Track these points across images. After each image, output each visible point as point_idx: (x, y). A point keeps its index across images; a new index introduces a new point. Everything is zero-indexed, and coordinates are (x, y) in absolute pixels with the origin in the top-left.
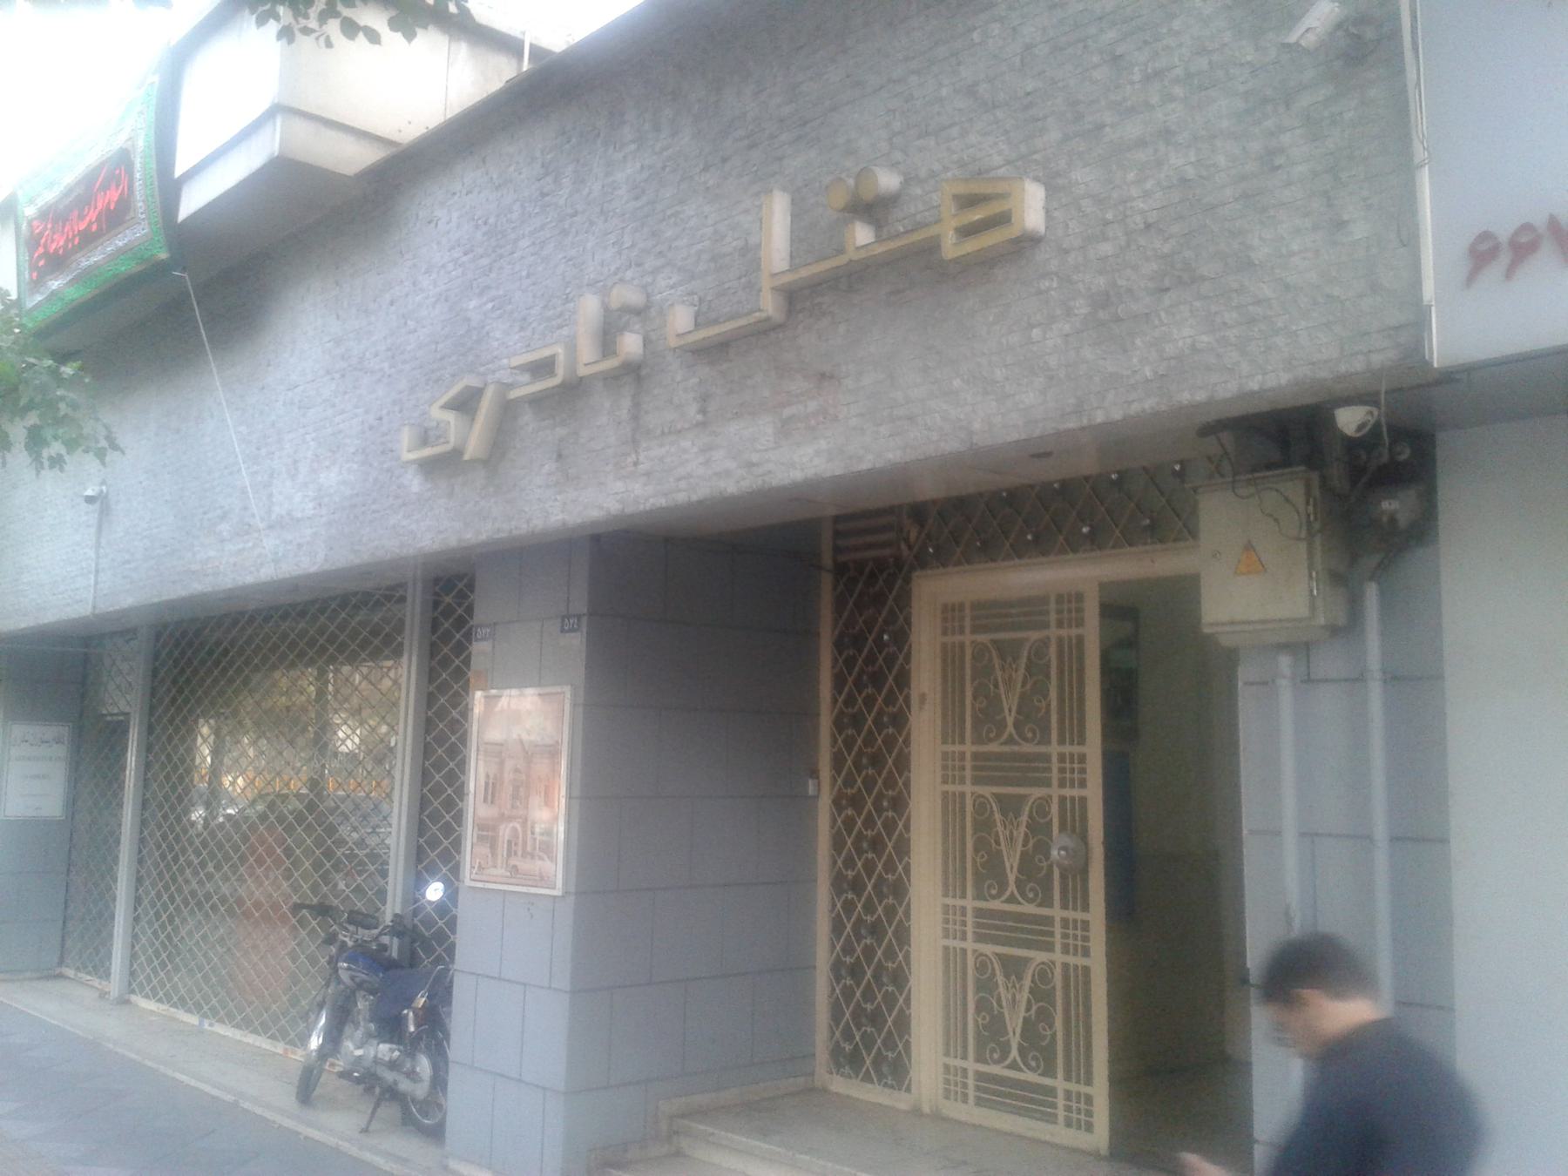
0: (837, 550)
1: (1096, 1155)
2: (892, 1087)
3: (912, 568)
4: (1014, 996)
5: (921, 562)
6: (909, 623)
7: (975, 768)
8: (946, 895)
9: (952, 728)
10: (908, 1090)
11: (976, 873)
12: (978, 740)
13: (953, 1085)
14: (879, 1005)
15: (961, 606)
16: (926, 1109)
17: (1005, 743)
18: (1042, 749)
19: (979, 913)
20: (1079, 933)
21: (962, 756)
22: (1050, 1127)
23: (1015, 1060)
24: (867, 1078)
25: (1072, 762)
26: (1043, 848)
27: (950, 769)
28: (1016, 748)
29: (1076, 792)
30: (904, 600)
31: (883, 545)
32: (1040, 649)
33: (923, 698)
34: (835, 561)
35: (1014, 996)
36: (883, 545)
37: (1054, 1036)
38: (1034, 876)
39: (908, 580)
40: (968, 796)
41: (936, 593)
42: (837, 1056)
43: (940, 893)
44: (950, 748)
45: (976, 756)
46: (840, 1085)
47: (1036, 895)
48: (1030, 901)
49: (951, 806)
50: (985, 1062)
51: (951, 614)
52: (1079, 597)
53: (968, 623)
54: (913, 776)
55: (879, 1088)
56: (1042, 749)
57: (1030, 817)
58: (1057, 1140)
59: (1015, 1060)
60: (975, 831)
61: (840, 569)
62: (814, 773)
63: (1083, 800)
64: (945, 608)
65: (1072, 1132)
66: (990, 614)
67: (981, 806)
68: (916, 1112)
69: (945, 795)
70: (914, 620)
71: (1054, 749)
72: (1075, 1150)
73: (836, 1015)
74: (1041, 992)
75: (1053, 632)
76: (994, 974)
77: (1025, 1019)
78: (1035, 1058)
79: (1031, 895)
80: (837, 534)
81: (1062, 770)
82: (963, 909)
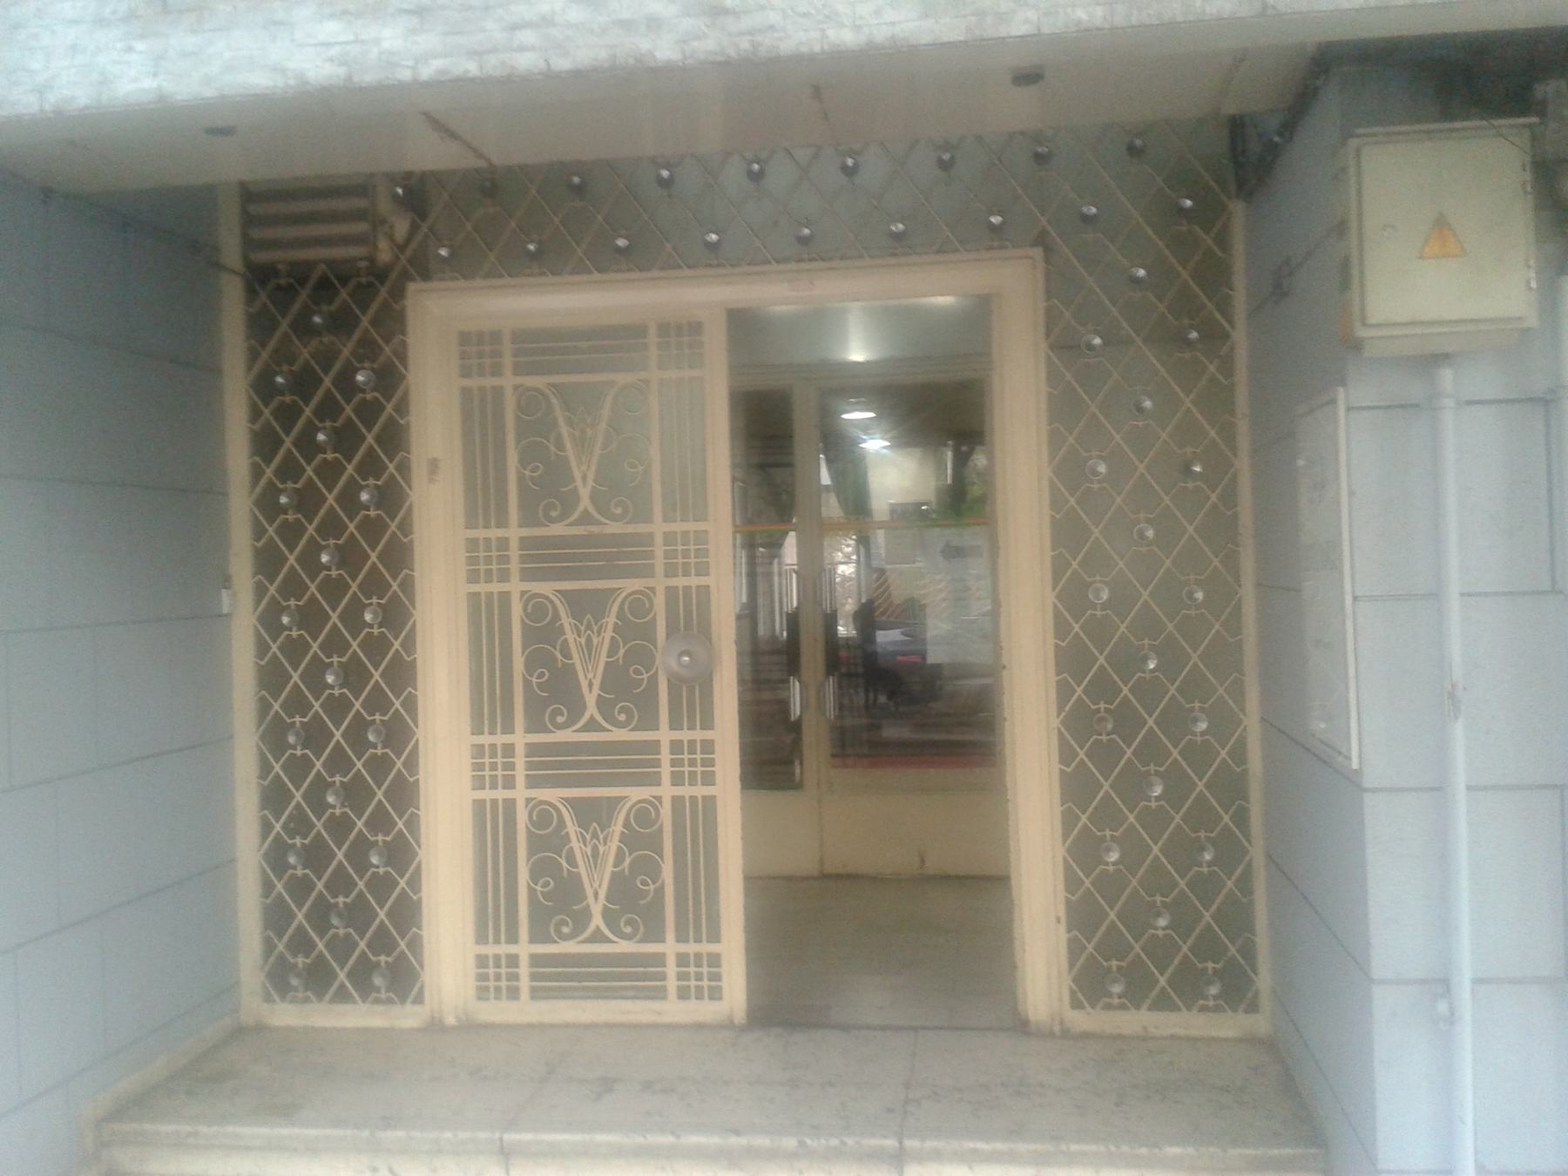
0: (249, 243)
1: (728, 1025)
2: (390, 1001)
3: (406, 276)
4: (595, 849)
5: (422, 268)
6: (403, 358)
7: (523, 559)
8: (469, 526)
9: (483, 501)
10: (419, 1000)
11: (523, 490)
12: (535, 725)
13: (493, 978)
14: (361, 894)
15: (496, 337)
16: (451, 1020)
17: (578, 523)
18: (641, 528)
19: (536, 960)
20: (705, 970)
21: (503, 543)
22: (655, 1005)
23: (586, 511)
24: (342, 996)
25: (698, 965)
26: (643, 657)
27: (481, 561)
28: (595, 529)
29: (700, 791)
30: (393, 321)
31: (346, 240)
32: (645, 815)
33: (434, 465)
34: (246, 259)
35: (595, 849)
36: (346, 240)
37: (660, 891)
38: (628, 691)
39: (398, 293)
40: (520, 805)
41: (446, 323)
42: (279, 980)
43: (461, 520)
44: (490, 950)
45: (532, 749)
46: (287, 1015)
47: (630, 718)
48: (628, 937)
49: (485, 620)
50: (547, 940)
51: (477, 349)
52: (696, 328)
53: (508, 360)
54: (411, 340)
55: (363, 1007)
56: (641, 528)
57: (627, 824)
58: (666, 1019)
59: (586, 511)
60: (532, 851)
61: (259, 277)
62: (226, 581)
63: (710, 801)
64: (465, 338)
65: (692, 1004)
66: (543, 348)
67: (537, 609)
68: (435, 1026)
69: (474, 598)
70: (412, 354)
71: (670, 947)
72: (699, 1027)
73: (276, 918)
74: (641, 835)
75: (666, 791)
76: (556, 617)
77: (614, 875)
78: (629, 922)
79: (628, 930)
80: (248, 221)
81: (681, 977)
82: (513, 960)
